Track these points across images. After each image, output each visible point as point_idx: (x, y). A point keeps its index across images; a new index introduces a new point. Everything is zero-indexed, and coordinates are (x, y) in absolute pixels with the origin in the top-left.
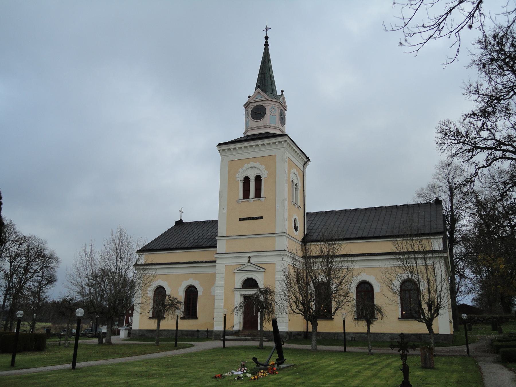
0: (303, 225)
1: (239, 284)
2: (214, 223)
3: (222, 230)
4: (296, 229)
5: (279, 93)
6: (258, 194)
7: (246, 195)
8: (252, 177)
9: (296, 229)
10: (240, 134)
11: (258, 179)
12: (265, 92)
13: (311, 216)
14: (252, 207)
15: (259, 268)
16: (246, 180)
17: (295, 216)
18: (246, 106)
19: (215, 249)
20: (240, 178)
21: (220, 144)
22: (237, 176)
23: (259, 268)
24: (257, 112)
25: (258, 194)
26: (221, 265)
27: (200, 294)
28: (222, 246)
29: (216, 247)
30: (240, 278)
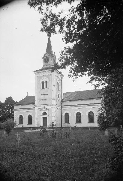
0: (63, 86)
1: (41, 114)
2: (34, 97)
3: (36, 99)
4: (59, 97)
5: (54, 53)
6: (46, 87)
7: (43, 87)
8: (45, 81)
9: (59, 97)
10: (41, 68)
11: (46, 82)
12: (48, 53)
13: (64, 93)
14: (44, 91)
15: (47, 109)
16: (43, 83)
17: (58, 94)
18: (43, 58)
19: (34, 110)
20: (41, 82)
21: (35, 71)
22: (40, 81)
23: (47, 109)
24: (46, 60)
25: (46, 87)
26: (37, 108)
27: (32, 117)
28: (36, 103)
29: (35, 104)
30: (42, 112)
